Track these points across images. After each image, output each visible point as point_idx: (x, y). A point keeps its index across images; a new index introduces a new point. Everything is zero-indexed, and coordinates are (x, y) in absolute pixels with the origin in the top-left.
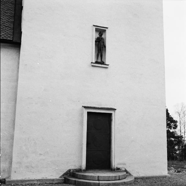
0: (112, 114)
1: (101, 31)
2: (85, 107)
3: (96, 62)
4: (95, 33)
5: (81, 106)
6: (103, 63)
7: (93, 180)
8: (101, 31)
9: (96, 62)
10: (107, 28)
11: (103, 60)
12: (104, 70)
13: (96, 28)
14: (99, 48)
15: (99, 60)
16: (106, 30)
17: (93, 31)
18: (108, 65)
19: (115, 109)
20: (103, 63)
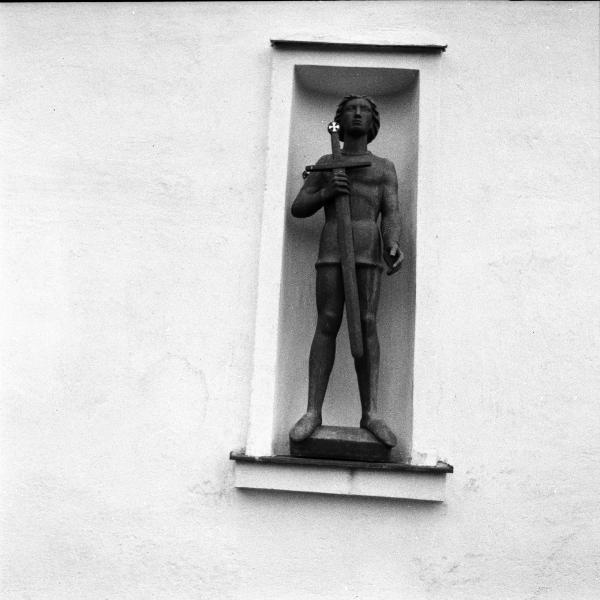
0: (418, 71)
1: (346, 434)
2: (281, 46)
3: (306, 450)
4: (287, 119)
5: (268, 45)
6: (377, 453)
7: (334, 459)
8: (346, 434)
9: (306, 450)
10: (434, 51)
11: (374, 416)
12: (390, 528)
13: (298, 69)
14: (331, 275)
15: (342, 416)
16: (412, 78)
17: (267, 92)
18: (440, 472)
19: (443, 49)
20: (377, 453)
